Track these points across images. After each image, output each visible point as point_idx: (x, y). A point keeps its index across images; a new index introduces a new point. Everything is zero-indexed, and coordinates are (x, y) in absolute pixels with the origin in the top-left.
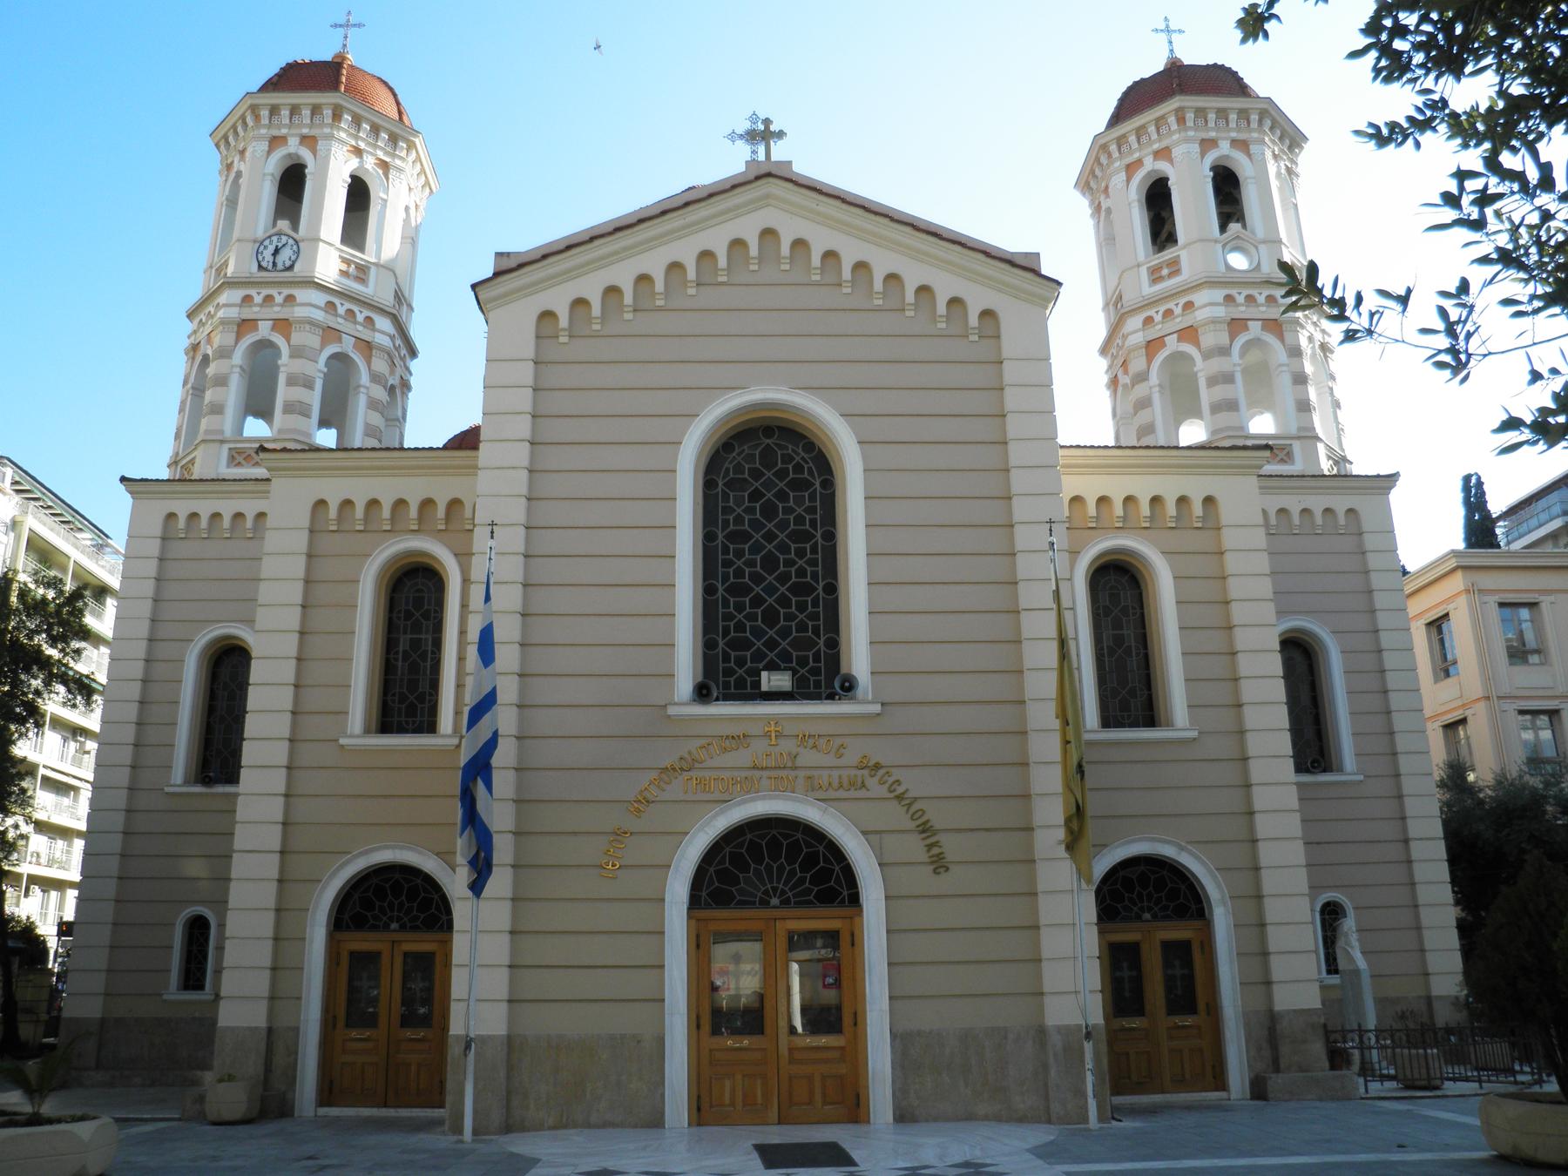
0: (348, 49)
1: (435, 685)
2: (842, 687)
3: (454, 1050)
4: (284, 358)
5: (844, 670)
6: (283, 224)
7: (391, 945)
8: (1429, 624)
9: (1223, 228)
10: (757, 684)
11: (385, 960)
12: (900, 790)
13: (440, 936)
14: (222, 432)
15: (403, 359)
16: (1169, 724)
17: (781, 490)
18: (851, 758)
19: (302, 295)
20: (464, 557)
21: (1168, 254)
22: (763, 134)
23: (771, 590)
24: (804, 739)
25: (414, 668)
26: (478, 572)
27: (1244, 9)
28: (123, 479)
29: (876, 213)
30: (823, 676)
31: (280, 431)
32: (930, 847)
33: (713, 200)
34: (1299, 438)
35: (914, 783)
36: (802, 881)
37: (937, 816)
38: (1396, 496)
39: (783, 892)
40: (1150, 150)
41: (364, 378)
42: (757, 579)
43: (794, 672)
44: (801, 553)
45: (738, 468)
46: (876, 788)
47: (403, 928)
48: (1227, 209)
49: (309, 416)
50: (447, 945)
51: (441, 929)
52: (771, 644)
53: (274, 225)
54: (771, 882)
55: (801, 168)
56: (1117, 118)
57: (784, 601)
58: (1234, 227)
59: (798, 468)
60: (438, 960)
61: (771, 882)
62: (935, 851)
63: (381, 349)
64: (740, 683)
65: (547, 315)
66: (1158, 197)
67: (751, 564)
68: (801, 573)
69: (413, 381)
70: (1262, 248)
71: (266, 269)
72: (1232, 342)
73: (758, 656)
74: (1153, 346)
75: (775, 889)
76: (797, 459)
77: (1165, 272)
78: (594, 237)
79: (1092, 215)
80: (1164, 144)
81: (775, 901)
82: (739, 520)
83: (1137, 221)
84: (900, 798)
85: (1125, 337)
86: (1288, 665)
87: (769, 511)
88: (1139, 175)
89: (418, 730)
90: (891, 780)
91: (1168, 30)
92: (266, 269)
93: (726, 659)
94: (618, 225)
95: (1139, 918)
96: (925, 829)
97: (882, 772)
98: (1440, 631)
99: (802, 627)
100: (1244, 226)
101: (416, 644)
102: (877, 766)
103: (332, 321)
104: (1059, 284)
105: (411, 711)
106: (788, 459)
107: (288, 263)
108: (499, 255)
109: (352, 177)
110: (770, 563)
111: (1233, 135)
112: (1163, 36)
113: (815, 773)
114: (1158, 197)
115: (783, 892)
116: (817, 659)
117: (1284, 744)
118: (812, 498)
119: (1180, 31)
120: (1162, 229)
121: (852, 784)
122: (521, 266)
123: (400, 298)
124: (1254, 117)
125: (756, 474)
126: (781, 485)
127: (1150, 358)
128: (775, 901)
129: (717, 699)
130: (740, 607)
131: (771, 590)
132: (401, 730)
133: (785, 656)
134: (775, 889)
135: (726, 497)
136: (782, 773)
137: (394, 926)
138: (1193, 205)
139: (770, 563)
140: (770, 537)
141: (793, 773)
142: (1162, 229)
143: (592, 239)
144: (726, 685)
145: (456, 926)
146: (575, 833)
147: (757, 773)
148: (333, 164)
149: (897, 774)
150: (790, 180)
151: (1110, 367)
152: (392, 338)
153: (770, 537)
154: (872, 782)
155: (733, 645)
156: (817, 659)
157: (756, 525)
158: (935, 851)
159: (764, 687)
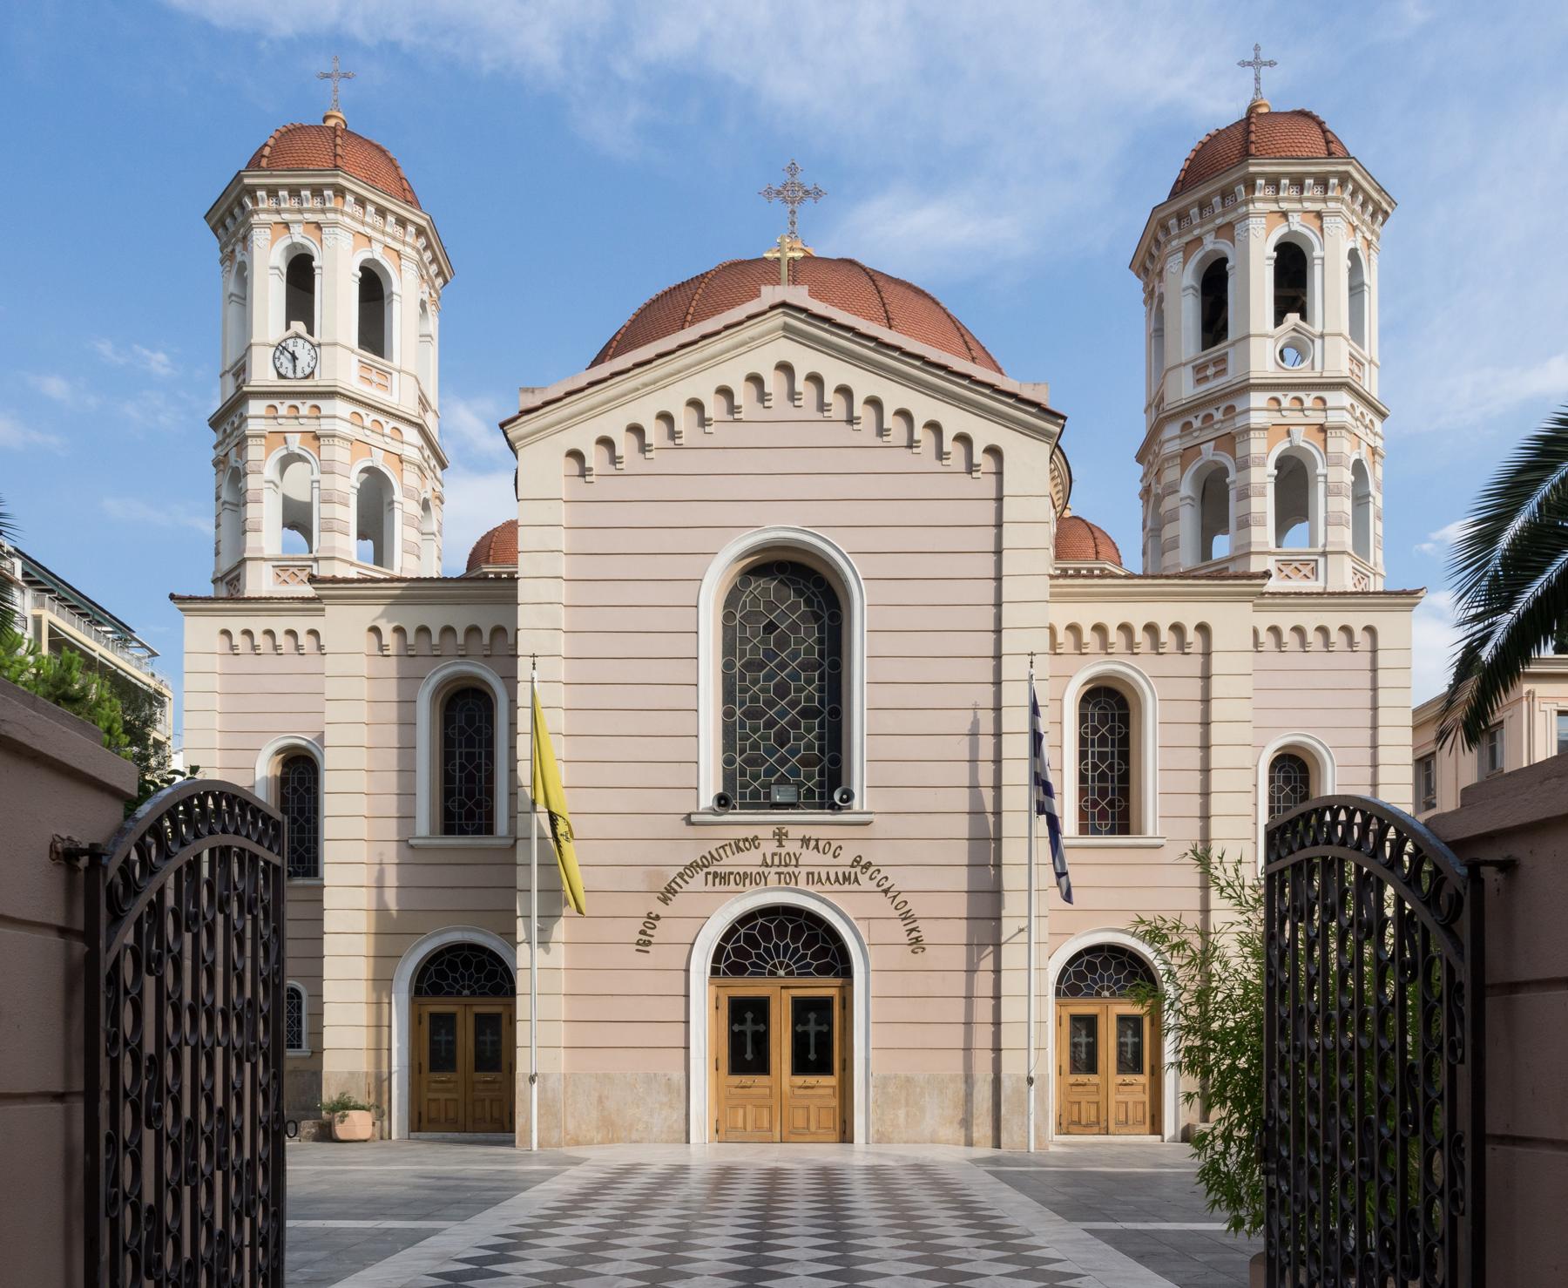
1: (490, 793)
3: (520, 1084)
6: (299, 326)
7: (464, 1009)
9: (1279, 319)
10: (768, 796)
11: (460, 1019)
13: (506, 1000)
18: (846, 857)
20: (511, 679)
21: (1215, 351)
24: (805, 841)
25: (470, 778)
26: (523, 698)
28: (172, 597)
30: (827, 782)
36: (804, 956)
37: (917, 906)
39: (788, 965)
40: (1211, 226)
47: (473, 994)
48: (1291, 292)
50: (512, 1007)
51: (506, 994)
53: (288, 327)
56: (1175, 193)
60: (505, 1021)
62: (914, 934)
74: (1186, 456)
75: (781, 963)
77: (1210, 371)
79: (1145, 302)
80: (1228, 219)
83: (1186, 312)
84: (886, 892)
85: (1161, 444)
89: (478, 831)
91: (1256, 63)
95: (1098, 994)
96: (907, 917)
97: (872, 869)
100: (1304, 317)
101: (470, 757)
103: (359, 434)
104: (1065, 418)
105: (470, 815)
107: (308, 371)
109: (362, 269)
113: (816, 870)
115: (788, 965)
120: (1214, 324)
121: (846, 879)
128: (782, 973)
130: (755, 730)
132: (463, 832)
134: (781, 963)
136: (786, 869)
141: (796, 871)
142: (1214, 324)
144: (743, 796)
145: (519, 990)
147: (766, 870)
151: (1145, 475)
152: (420, 449)
154: (863, 878)
158: (914, 934)
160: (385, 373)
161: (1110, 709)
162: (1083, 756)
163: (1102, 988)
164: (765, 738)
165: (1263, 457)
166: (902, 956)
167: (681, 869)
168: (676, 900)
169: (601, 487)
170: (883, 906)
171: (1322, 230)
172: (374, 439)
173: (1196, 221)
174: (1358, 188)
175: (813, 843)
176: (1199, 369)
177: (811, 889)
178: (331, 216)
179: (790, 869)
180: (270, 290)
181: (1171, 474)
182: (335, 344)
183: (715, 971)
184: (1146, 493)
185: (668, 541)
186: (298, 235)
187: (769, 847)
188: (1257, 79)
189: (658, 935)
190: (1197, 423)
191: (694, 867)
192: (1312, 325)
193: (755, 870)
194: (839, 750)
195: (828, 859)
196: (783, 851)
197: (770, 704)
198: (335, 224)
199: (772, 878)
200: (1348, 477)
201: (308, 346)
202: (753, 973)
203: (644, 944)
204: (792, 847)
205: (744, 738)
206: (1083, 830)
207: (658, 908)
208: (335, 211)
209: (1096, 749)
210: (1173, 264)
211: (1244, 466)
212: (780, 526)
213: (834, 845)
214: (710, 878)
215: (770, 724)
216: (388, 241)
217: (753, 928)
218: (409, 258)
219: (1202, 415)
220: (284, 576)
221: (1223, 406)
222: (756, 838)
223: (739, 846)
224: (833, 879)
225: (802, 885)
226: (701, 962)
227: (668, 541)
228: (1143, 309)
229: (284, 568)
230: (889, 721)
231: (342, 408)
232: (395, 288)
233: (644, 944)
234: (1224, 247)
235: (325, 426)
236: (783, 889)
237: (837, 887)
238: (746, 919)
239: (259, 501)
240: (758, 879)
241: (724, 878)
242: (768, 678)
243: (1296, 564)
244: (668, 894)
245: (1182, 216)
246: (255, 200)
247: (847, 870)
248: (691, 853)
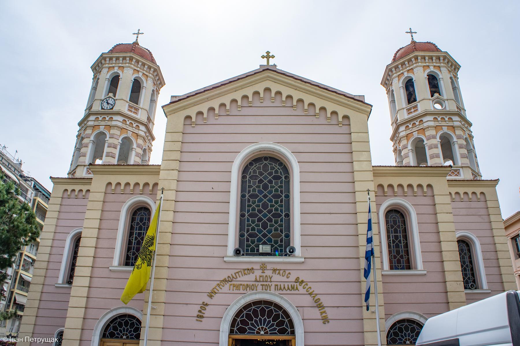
2: (290, 252)
4: (108, 138)
5: (291, 245)
6: (111, 95)
8: (512, 238)
10: (258, 250)
12: (311, 291)
14: (85, 162)
15: (149, 140)
16: (416, 268)
17: (270, 180)
18: (292, 278)
19: (115, 118)
22: (268, 56)
23: (265, 216)
24: (274, 270)
28: (51, 177)
29: (305, 82)
30: (283, 246)
31: (104, 162)
32: (321, 313)
33: (247, 78)
34: (462, 167)
35: (317, 288)
37: (325, 301)
38: (498, 187)
40: (406, 70)
41: (135, 146)
42: (260, 211)
43: (272, 246)
44: (276, 202)
45: (255, 172)
46: (301, 290)
49: (114, 158)
52: (265, 236)
54: (261, 325)
55: (279, 67)
57: (270, 220)
58: (436, 95)
59: (276, 172)
61: (261, 325)
62: (324, 315)
63: (141, 136)
64: (253, 250)
65: (188, 117)
66: (409, 85)
67: (258, 206)
68: (276, 209)
69: (153, 148)
70: (446, 101)
71: (104, 109)
72: (437, 133)
73: (259, 240)
76: (276, 168)
77: (413, 110)
78: (205, 90)
79: (387, 93)
81: (124, 337)
82: (254, 190)
83: (401, 95)
84: (310, 294)
85: (399, 133)
86: (461, 251)
87: (265, 187)
90: (307, 287)
91: (411, 32)
92: (104, 109)
93: (248, 240)
94: (215, 86)
96: (320, 306)
97: (304, 284)
98: (516, 241)
99: (276, 230)
100: (440, 95)
102: (302, 282)
104: (372, 106)
106: (273, 168)
108: (172, 97)
110: (265, 206)
111: (435, 64)
112: (410, 34)
113: (279, 284)
114: (409, 85)
115: (266, 329)
116: (281, 241)
117: (460, 276)
118: (281, 183)
119: (415, 33)
120: (411, 98)
121: (293, 288)
122: (180, 100)
123: (149, 119)
125: (261, 174)
126: (270, 178)
128: (262, 333)
129: (243, 255)
130: (253, 222)
131: (265, 216)
133: (270, 240)
134: (262, 328)
135: (250, 182)
137: (124, 337)
138: (422, 89)
139: (265, 206)
140: (265, 196)
141: (270, 284)
142: (411, 98)
143: (204, 91)
144: (247, 250)
146: (187, 304)
147: (257, 283)
149: (310, 285)
150: (275, 71)
152: (145, 133)
153: (265, 196)
154: (300, 288)
155: (250, 235)
156: (281, 241)
157: (260, 192)
158: (324, 315)
159: (261, 251)
160: (137, 109)
161: (397, 219)
162: (388, 237)
163: (406, 339)
164: (258, 225)
166: (318, 325)
167: (219, 282)
168: (216, 297)
171: (441, 71)
172: (130, 128)
173: (401, 69)
175: (277, 272)
176: (408, 110)
177: (277, 293)
179: (267, 283)
184: (395, 150)
187: (258, 273)
188: (412, 36)
189: (207, 313)
190: (410, 126)
191: (225, 281)
192: (443, 96)
193: (251, 283)
194: (289, 192)
196: (264, 275)
201: (113, 100)
202: (249, 333)
204: (268, 273)
205: (249, 225)
206: (391, 268)
209: (394, 234)
210: (395, 81)
212: (267, 144)
213: (287, 272)
214: (232, 287)
216: (145, 72)
217: (243, 317)
218: (150, 77)
219: (412, 123)
221: (419, 120)
222: (253, 269)
224: (286, 288)
225: (273, 291)
226: (225, 327)
232: (145, 85)
233: (200, 317)
234: (411, 75)
236: (263, 293)
237: (288, 292)
238: (247, 306)
240: (252, 288)
241: (237, 287)
242: (259, 201)
243: (452, 171)
245: (396, 67)
246: (105, 60)
247: (293, 284)
248: (224, 275)
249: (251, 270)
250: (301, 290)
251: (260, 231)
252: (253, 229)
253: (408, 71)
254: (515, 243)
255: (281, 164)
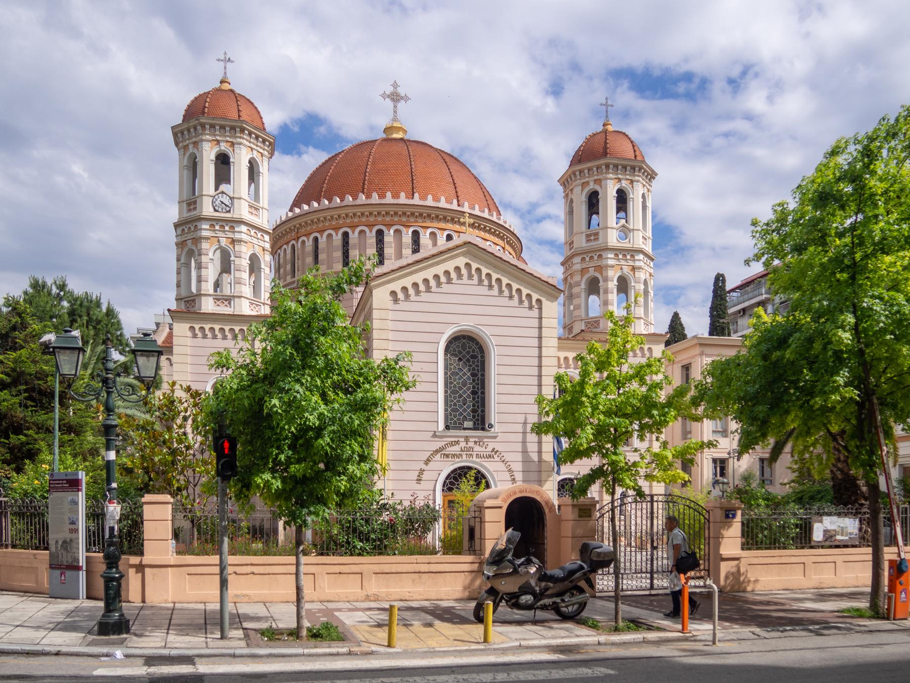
0: (228, 75)
8: (683, 366)
18: (490, 448)
27: (591, 469)
30: (480, 421)
46: (496, 458)
48: (620, 205)
74: (583, 271)
77: (592, 238)
83: (581, 209)
88: (586, 190)
96: (510, 471)
121: (490, 456)
124: (637, 169)
127: (582, 276)
148: (242, 157)
164: (458, 401)
165: (613, 275)
169: (403, 305)
170: (502, 466)
174: (645, 171)
178: (239, 140)
180: (208, 170)
181: (577, 278)
182: (240, 198)
183: (443, 490)
185: (427, 328)
186: (224, 147)
187: (463, 444)
189: (424, 477)
190: (587, 259)
191: (437, 452)
195: (483, 449)
197: (461, 389)
198: (240, 144)
199: (464, 456)
200: (642, 287)
203: (419, 480)
204: (471, 444)
207: (424, 467)
208: (240, 137)
210: (577, 190)
211: (606, 280)
212: (466, 324)
215: (461, 396)
220: (218, 303)
223: (452, 444)
227: (427, 328)
228: (563, 201)
229: (218, 300)
230: (504, 399)
231: (244, 228)
233: (419, 480)
234: (597, 188)
235: (237, 236)
239: (207, 268)
241: (447, 456)
242: (459, 379)
244: (427, 462)
249: (457, 443)
250: (496, 458)
251: (461, 407)
252: (455, 404)
253: (595, 181)
254: (685, 373)
255: (477, 343)
